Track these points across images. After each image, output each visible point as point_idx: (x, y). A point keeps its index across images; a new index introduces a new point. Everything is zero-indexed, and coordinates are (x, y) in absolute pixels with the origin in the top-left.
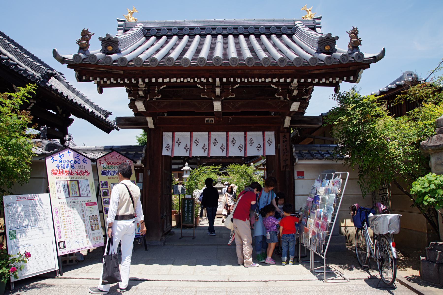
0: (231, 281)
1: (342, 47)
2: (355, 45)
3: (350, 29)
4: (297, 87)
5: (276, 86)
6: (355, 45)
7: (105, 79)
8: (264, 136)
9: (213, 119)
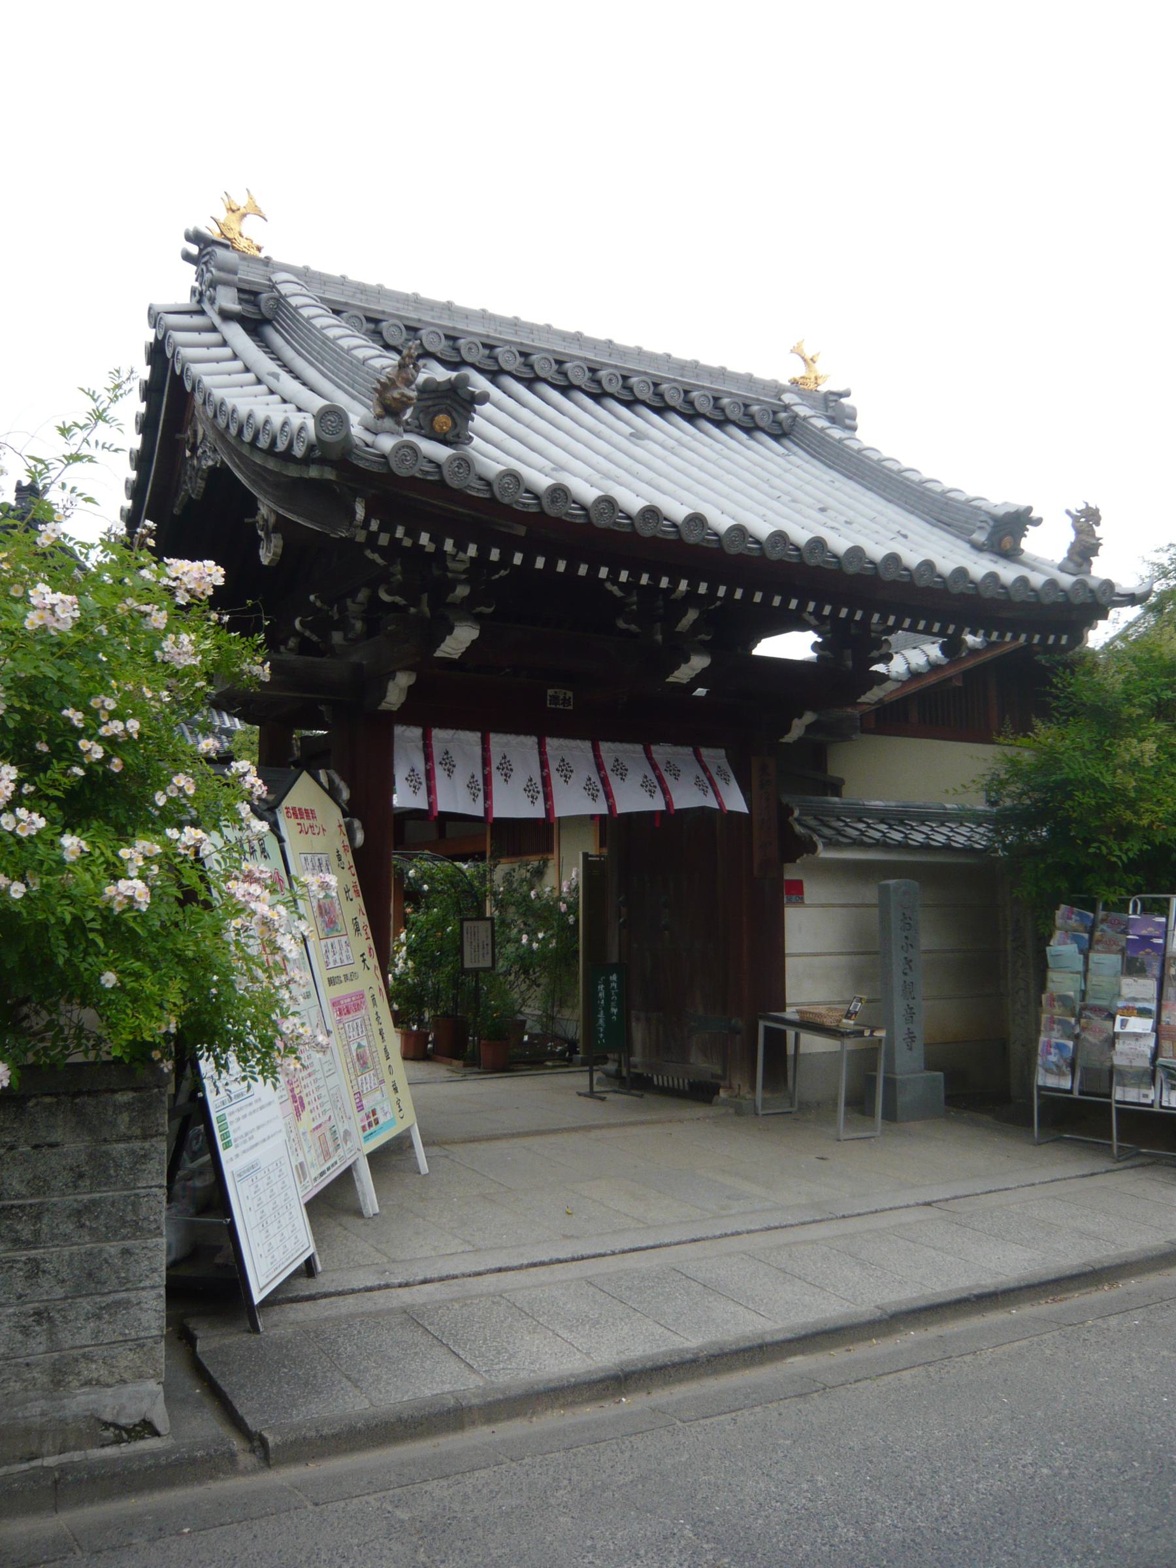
0: (844, 1217)
1: (1047, 546)
2: (1084, 550)
3: (1077, 506)
4: (465, 572)
5: (382, 558)
6: (1084, 550)
7: (400, 532)
8: (542, 753)
9: (570, 694)
